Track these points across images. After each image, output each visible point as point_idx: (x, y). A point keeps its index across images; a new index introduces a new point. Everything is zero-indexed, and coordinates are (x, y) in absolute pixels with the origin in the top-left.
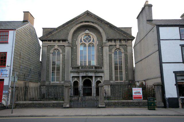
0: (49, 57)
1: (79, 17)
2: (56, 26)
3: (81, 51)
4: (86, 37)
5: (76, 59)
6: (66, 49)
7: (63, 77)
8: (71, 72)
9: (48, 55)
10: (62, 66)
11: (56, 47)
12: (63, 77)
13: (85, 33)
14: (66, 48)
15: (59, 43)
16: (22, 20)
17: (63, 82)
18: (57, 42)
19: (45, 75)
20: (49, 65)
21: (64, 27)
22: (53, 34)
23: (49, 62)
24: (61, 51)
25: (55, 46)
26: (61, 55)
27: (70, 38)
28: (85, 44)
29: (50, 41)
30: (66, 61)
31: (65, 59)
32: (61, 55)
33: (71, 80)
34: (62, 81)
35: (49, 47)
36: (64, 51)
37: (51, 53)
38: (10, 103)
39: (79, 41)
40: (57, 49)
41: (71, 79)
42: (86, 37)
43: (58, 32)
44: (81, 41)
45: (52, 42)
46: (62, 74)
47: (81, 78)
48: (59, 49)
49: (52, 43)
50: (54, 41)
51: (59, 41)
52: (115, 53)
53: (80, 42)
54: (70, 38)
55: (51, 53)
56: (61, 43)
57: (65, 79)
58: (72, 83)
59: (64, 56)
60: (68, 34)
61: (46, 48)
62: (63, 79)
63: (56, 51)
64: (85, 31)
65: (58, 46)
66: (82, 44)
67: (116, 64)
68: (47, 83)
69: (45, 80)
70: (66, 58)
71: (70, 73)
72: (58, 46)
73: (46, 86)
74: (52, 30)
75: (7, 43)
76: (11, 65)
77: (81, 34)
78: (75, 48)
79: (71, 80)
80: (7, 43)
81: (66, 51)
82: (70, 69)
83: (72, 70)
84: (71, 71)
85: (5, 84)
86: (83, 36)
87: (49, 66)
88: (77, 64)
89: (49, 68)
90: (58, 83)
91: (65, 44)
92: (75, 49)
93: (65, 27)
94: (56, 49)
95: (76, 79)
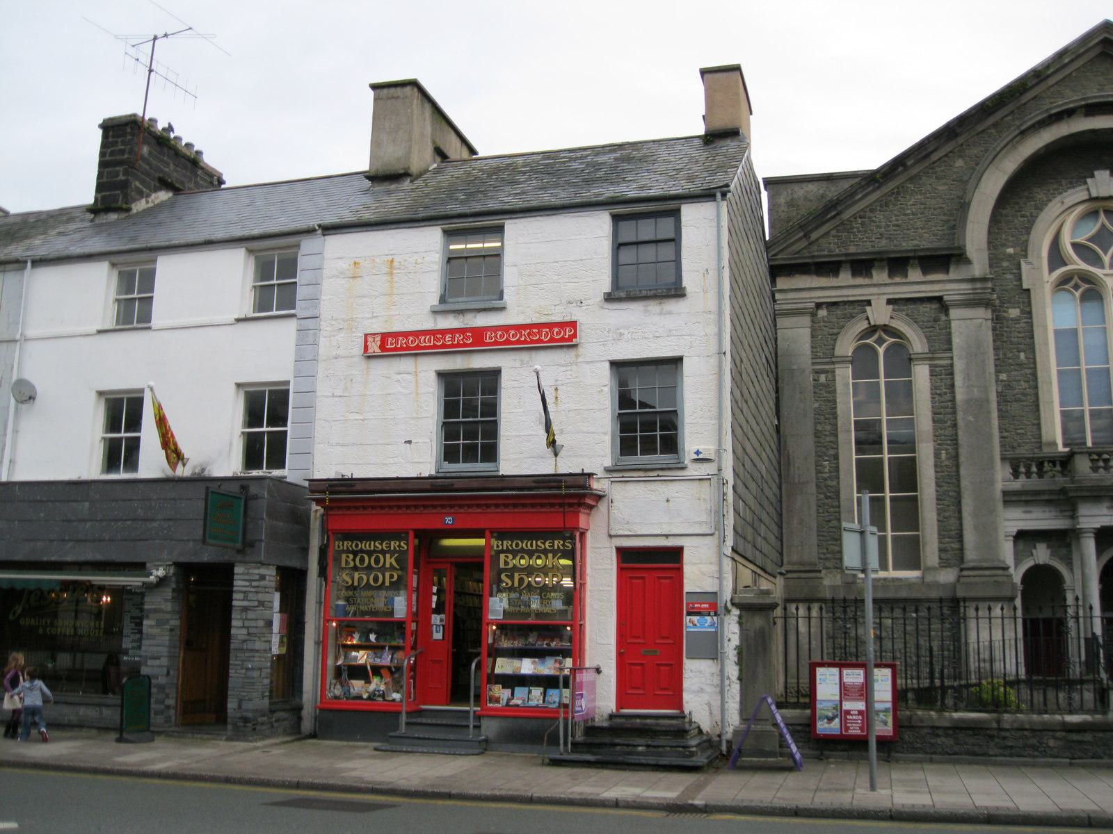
0: (830, 388)
1: (1037, 76)
2: (873, 159)
3: (1068, 338)
4: (1092, 228)
5: (1031, 399)
6: (954, 324)
7: (952, 535)
8: (1011, 499)
9: (818, 372)
10: (937, 455)
11: (880, 313)
12: (952, 535)
13: (1084, 196)
14: (954, 313)
15: (897, 280)
16: (701, 131)
17: (947, 576)
18: (880, 276)
19: (814, 525)
20: (835, 445)
21: (927, 163)
22: (846, 215)
23: (835, 425)
24: (918, 344)
25: (869, 303)
26: (921, 375)
27: (975, 237)
28: (1086, 278)
29: (828, 268)
30: (960, 415)
31: (953, 400)
32: (921, 375)
33: (1010, 561)
34: (944, 564)
35: (823, 313)
36: (942, 341)
37: (843, 360)
38: (744, 719)
39: (1039, 256)
40: (886, 329)
41: (1007, 551)
42: (1092, 228)
43: (884, 204)
44: (1056, 258)
45: (845, 277)
46: (939, 512)
47: (1090, 545)
48: (898, 324)
49: (844, 286)
50: (862, 266)
51: (898, 264)
52: (863, 361)
53: (1051, 270)
54: (975, 237)
55: (843, 360)
56: (917, 283)
57: (971, 555)
58: (1017, 576)
59: (943, 377)
60: (963, 207)
61: (807, 320)
62: (953, 553)
63: (880, 341)
64: (1082, 180)
65: (890, 302)
66: (1064, 281)
67: (868, 439)
68: (826, 582)
69: (815, 559)
70: (960, 396)
71: (1000, 505)
72: (890, 302)
73: (824, 601)
74: (833, 192)
75: (676, 292)
76: (719, 452)
77: (1053, 208)
78: (1014, 313)
79: (1010, 561)
80: (676, 292)
81: (956, 341)
82: (1002, 477)
83: (1017, 485)
84: (1005, 493)
85: (688, 587)
86: (1071, 219)
87: (836, 457)
88: (1045, 437)
89: (837, 469)
90: (908, 584)
91: (947, 285)
92: (1016, 320)
93: (934, 157)
94: (873, 330)
95: (1042, 555)
